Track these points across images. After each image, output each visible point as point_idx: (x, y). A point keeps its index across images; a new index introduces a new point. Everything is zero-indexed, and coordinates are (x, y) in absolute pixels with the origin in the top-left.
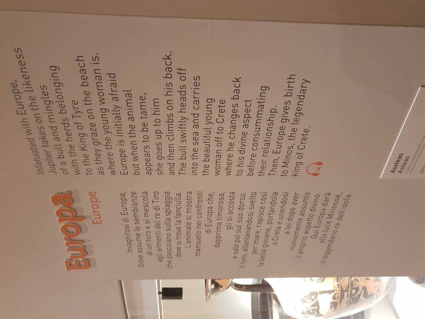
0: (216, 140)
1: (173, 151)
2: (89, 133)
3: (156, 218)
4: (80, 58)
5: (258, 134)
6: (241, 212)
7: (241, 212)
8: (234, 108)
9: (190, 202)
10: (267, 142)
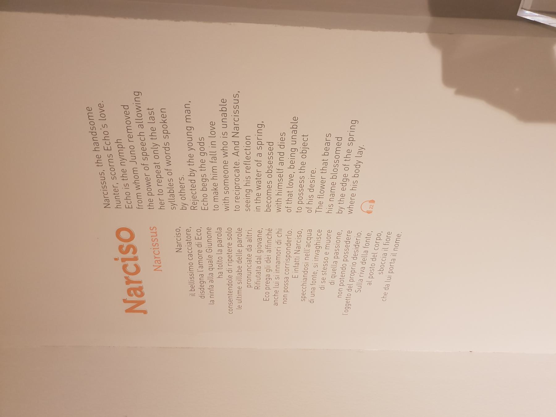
0: (266, 247)
4: (141, 134)
5: (338, 161)
6: (354, 261)
7: (354, 261)
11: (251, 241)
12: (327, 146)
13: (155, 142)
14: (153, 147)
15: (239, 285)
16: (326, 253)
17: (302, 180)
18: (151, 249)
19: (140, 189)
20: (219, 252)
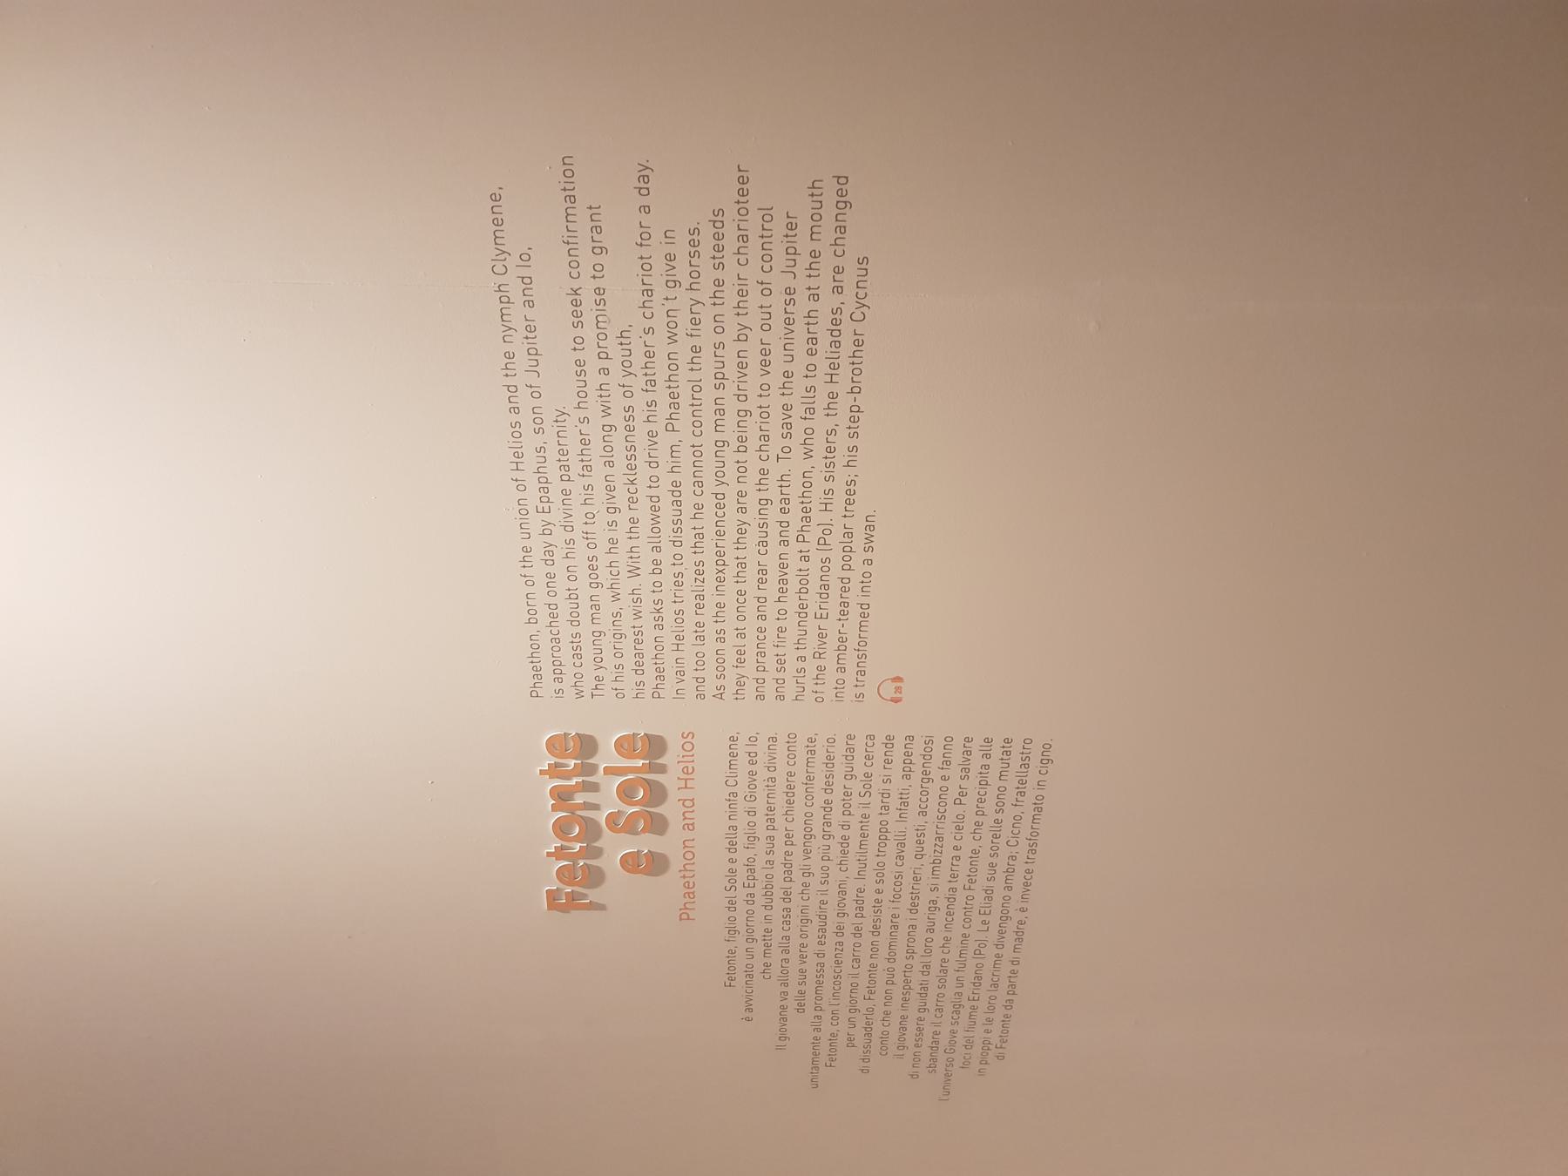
0: (585, 536)
2: (621, 424)
3: (885, 768)
9: (579, 648)
11: (786, 543)
12: (761, 576)
13: (743, 320)
14: (498, 258)
15: (992, 860)
17: (678, 526)
19: (610, 414)
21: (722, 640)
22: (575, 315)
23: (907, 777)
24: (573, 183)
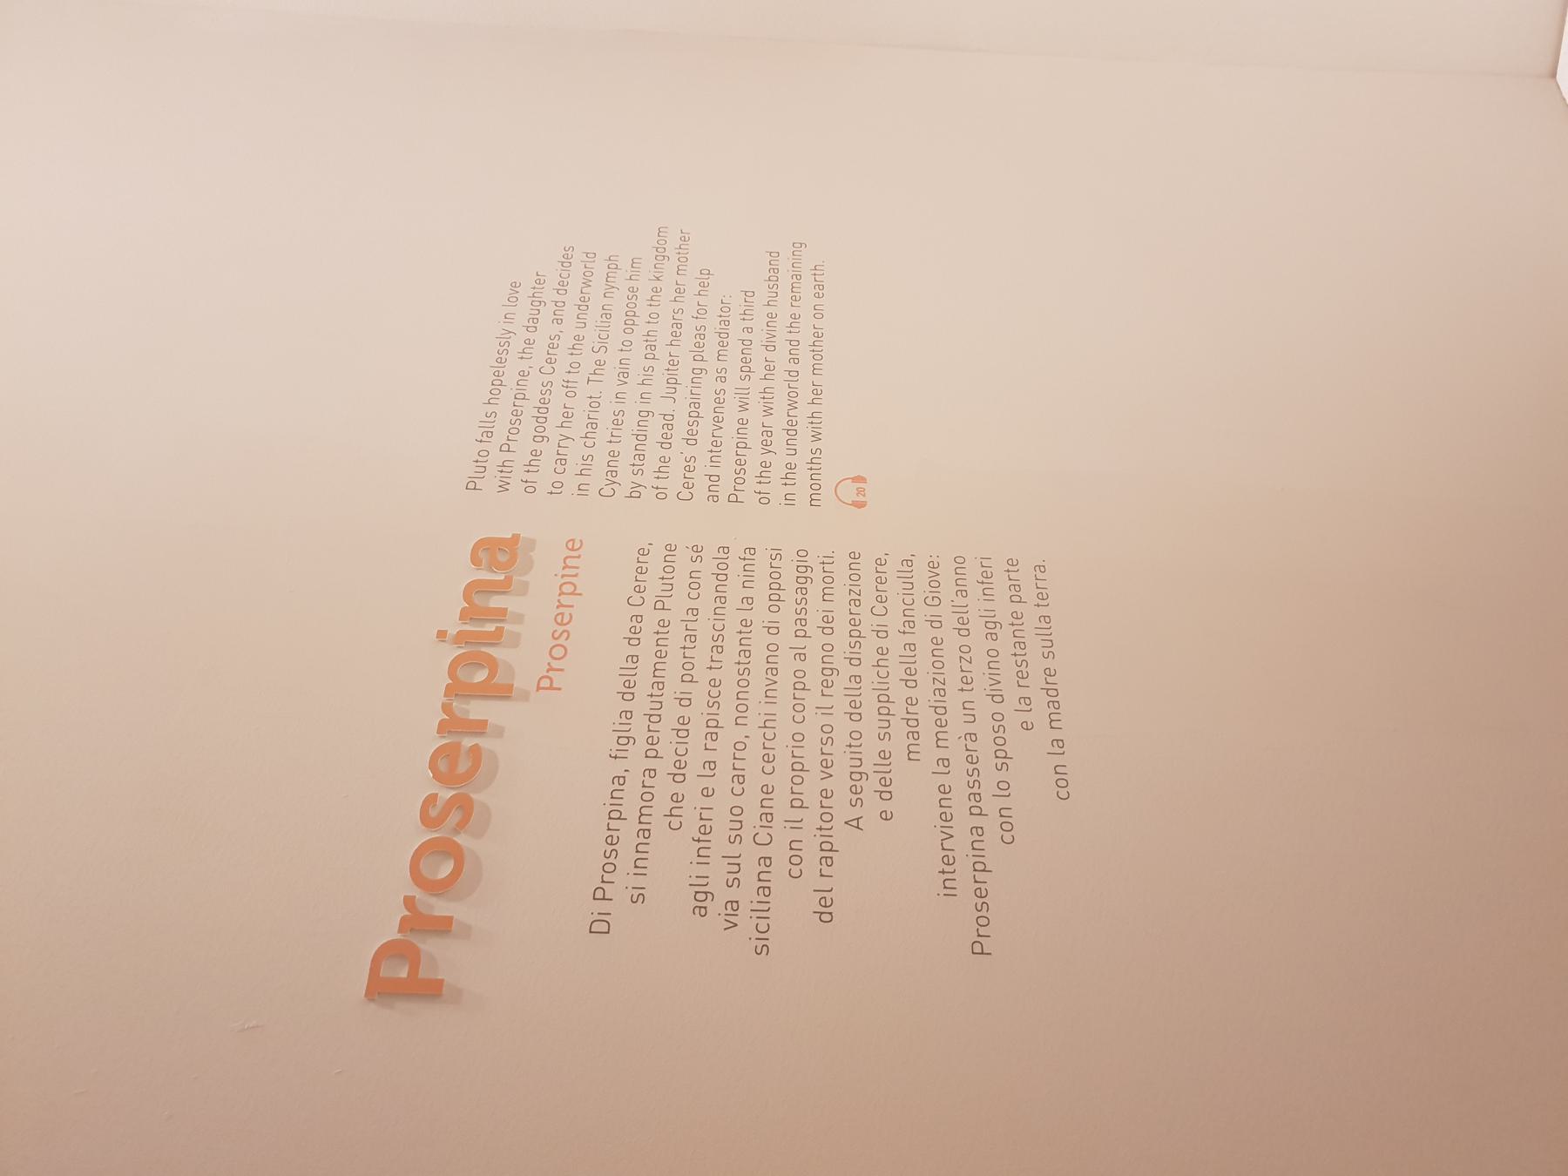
0: (565, 384)
1: (820, 335)
8: (688, 464)
10: (649, 343)
12: (634, 623)
16: (705, 792)
18: (556, 575)
20: (746, 606)
21: (724, 380)
22: (965, 681)
23: (671, 396)
24: (888, 683)
